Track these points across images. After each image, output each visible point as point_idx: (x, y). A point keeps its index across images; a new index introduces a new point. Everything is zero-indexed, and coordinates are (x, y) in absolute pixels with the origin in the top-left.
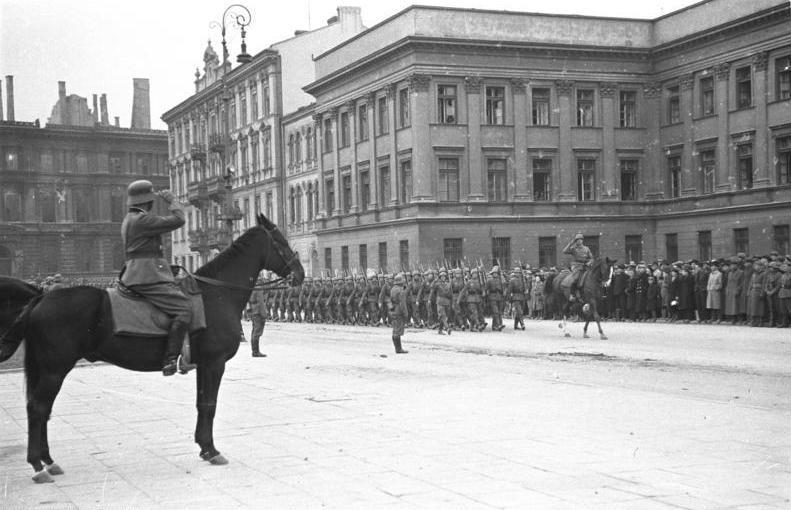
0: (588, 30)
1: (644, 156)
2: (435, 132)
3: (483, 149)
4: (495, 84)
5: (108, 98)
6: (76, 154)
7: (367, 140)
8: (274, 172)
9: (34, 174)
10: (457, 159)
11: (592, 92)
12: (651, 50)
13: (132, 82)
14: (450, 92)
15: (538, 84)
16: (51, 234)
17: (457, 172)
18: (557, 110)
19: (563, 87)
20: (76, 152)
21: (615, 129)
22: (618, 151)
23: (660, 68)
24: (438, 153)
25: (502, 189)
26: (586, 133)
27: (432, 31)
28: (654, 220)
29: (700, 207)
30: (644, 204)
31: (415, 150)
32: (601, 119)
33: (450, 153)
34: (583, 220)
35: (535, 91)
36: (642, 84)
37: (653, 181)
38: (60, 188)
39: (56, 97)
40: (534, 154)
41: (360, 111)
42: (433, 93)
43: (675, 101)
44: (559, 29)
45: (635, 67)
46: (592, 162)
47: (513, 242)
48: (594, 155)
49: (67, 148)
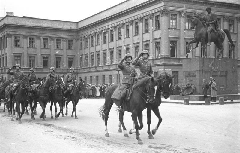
0: (59, 24)
1: (75, 57)
2: (14, 49)
3: (185, 38)
10: (20, 56)
11: (60, 40)
12: (76, 30)
14: (18, 39)
17: (20, 59)
18: (50, 44)
21: (67, 50)
23: (80, 34)
27: (12, 22)
28: (77, 73)
31: (162, 39)
35: (44, 39)
37: (77, 63)
40: (43, 56)
42: (13, 39)
43: (82, 43)
44: (51, 23)
45: (74, 34)
48: (61, 56)
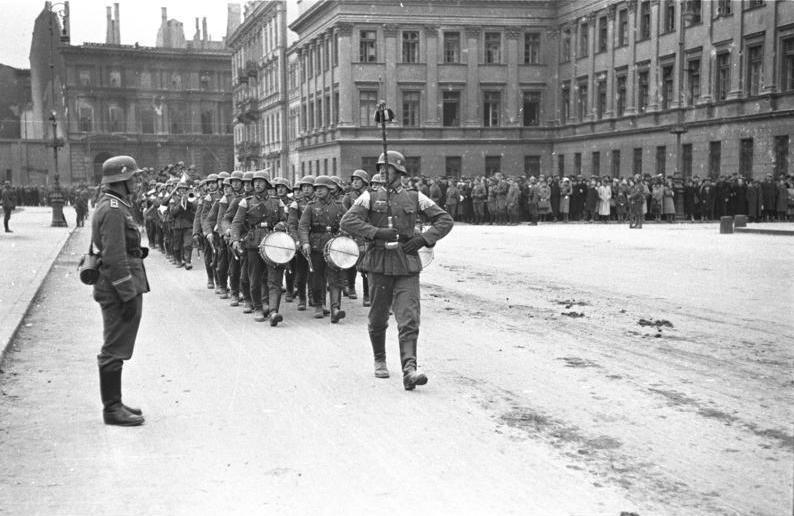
4: (411, 29)
5: (208, 21)
6: (172, 74)
7: (627, 45)
8: (280, 95)
9: (134, 91)
13: (227, 6)
14: (371, 36)
15: (449, 29)
16: (148, 144)
19: (472, 31)
20: (171, 71)
22: (522, 84)
24: (359, 87)
25: (416, 117)
26: (533, 69)
28: (551, 143)
29: (579, 133)
30: (544, 130)
32: (506, 57)
33: (368, 87)
34: (486, 143)
35: (447, 34)
36: (545, 27)
37: (550, 111)
38: (158, 102)
39: (159, 22)
40: (444, 87)
41: (621, 17)
42: (356, 37)
46: (497, 94)
47: (423, 160)
49: (162, 67)
